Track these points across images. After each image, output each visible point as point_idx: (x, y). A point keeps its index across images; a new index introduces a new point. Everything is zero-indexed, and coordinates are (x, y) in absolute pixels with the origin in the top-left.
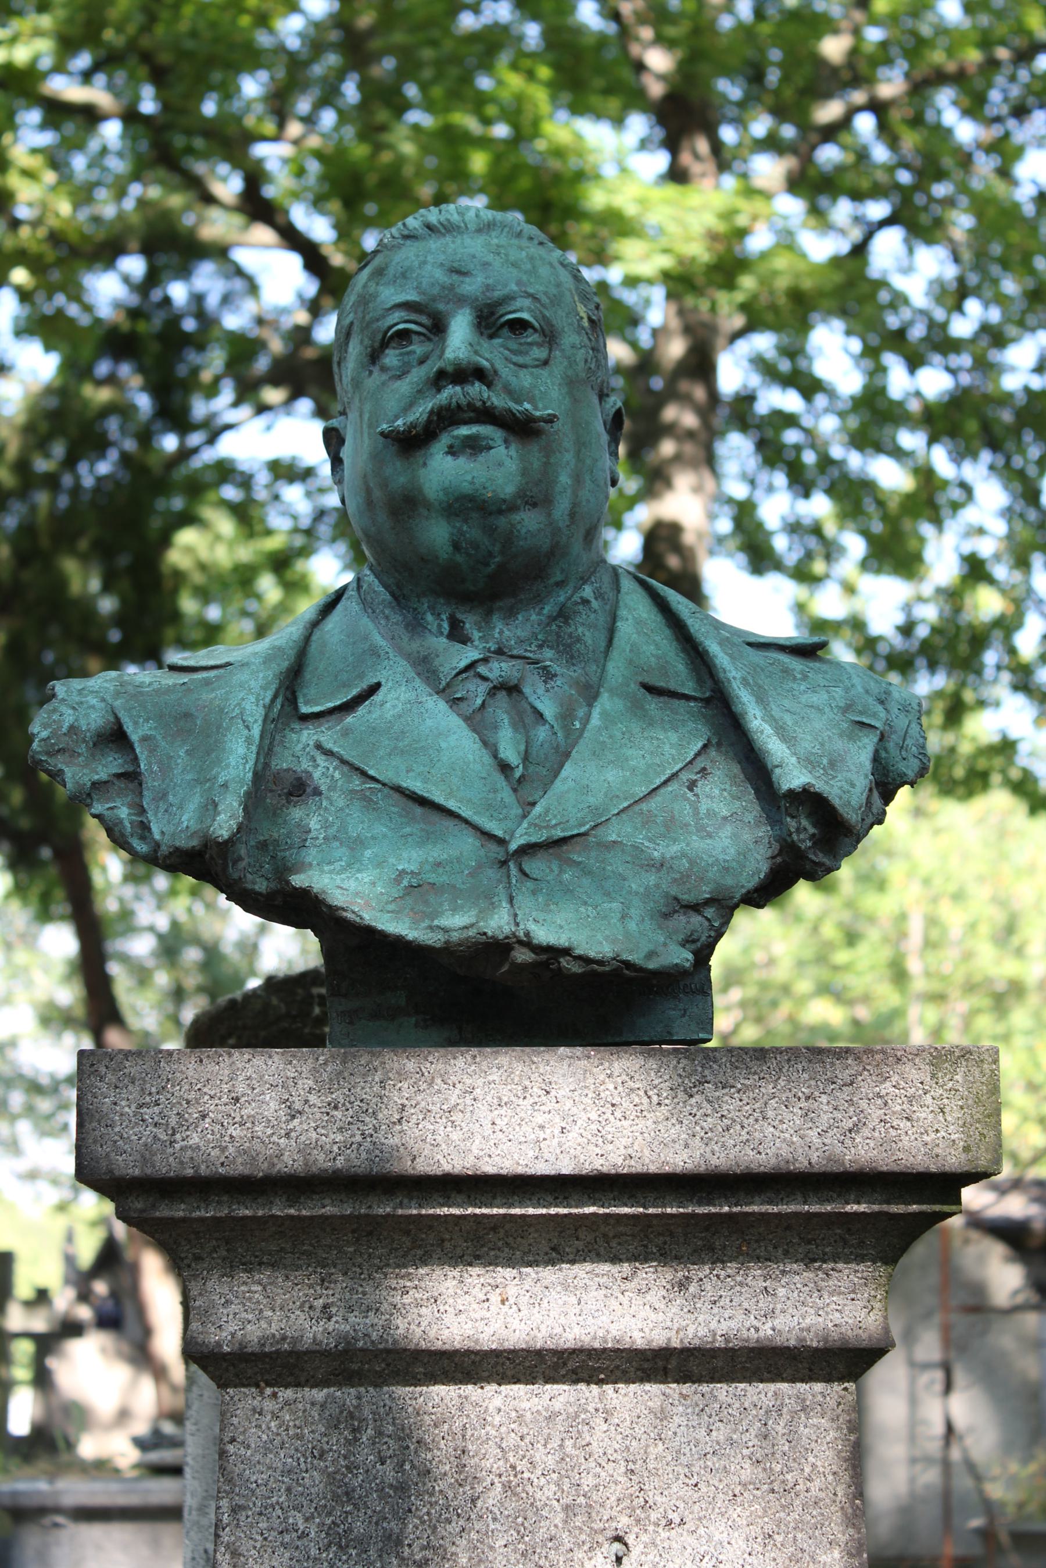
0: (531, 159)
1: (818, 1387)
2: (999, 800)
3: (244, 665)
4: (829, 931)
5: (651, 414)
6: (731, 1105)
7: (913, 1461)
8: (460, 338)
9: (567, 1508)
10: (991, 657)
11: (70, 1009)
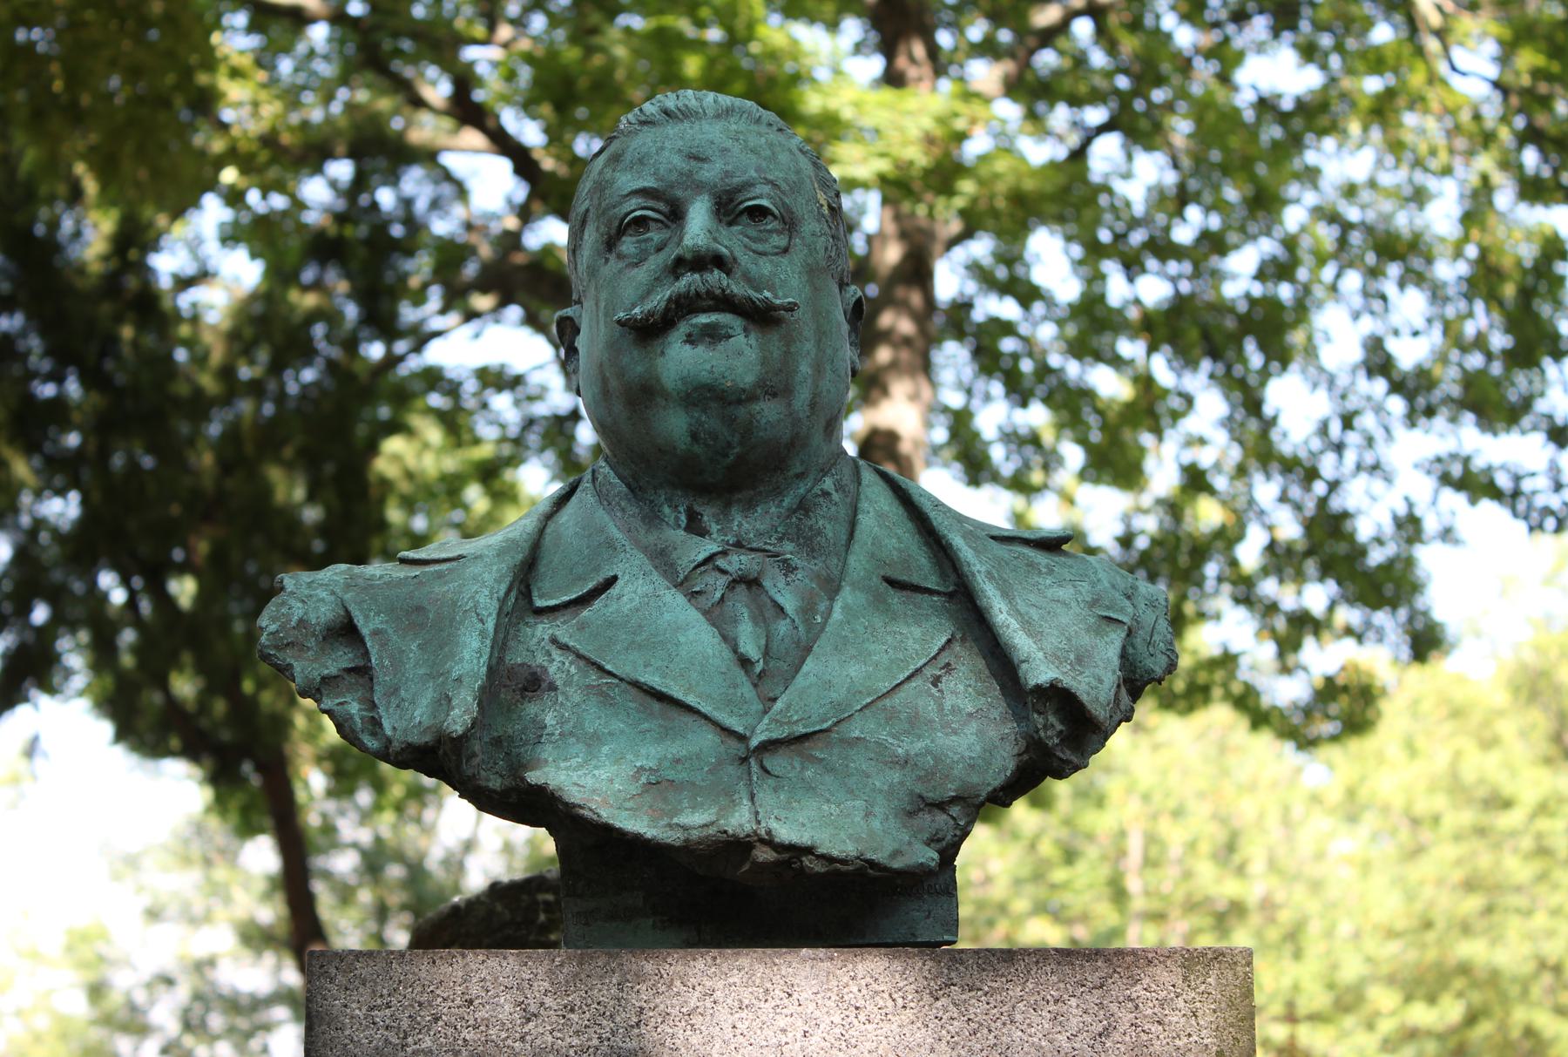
0: (745, 63)
2: (1219, 715)
3: (478, 557)
4: (1047, 848)
5: (883, 309)
6: (977, 1008)
8: (698, 224)
10: (1211, 569)
11: (271, 927)
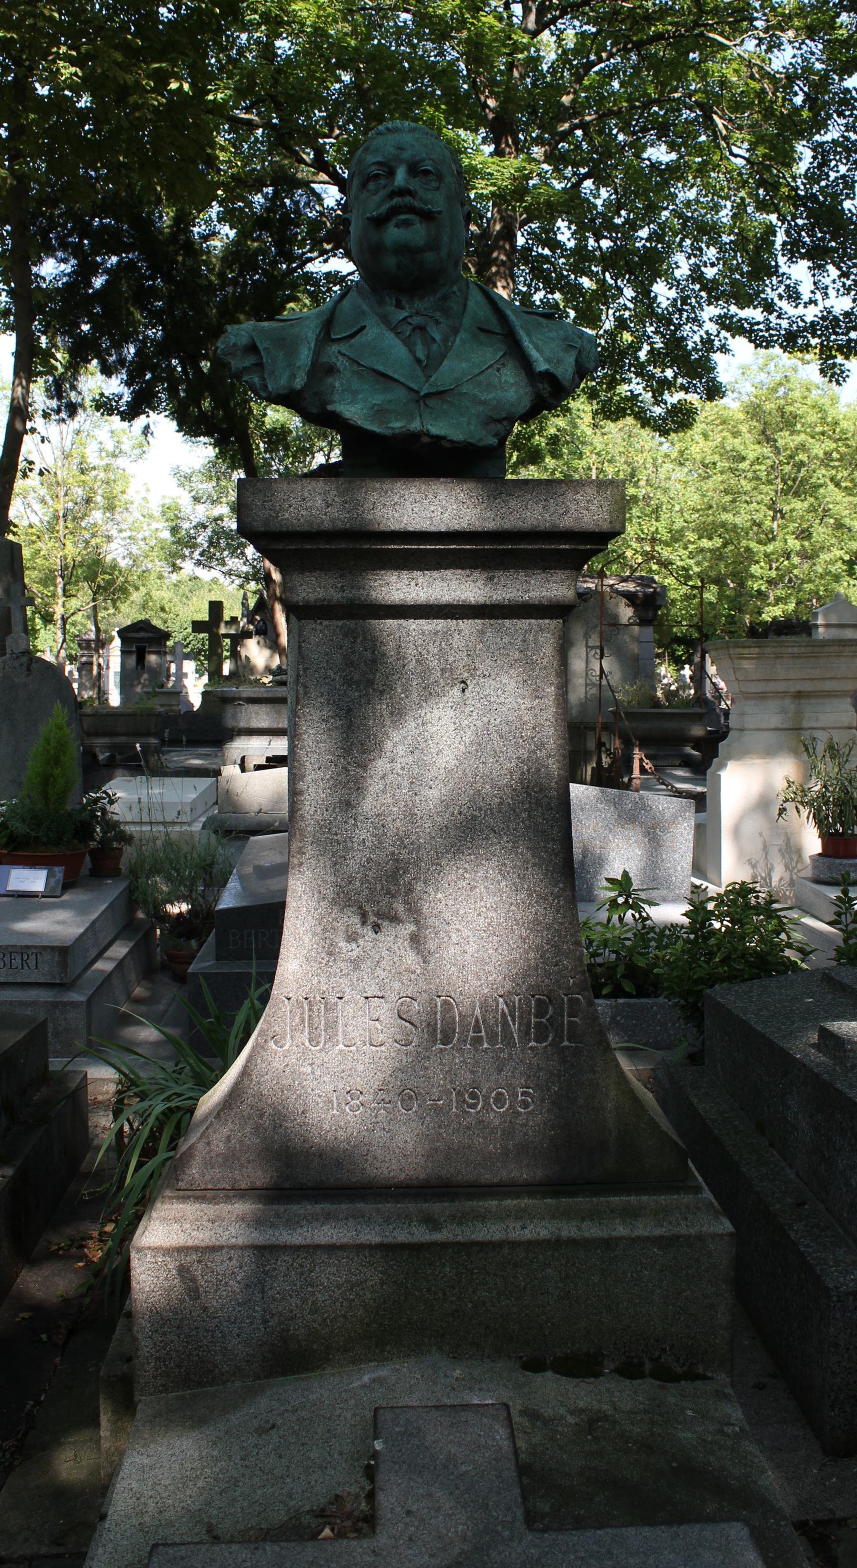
1: (547, 621)
5: (493, 250)
7: (587, 685)
8: (401, 176)
9: (442, 670)
